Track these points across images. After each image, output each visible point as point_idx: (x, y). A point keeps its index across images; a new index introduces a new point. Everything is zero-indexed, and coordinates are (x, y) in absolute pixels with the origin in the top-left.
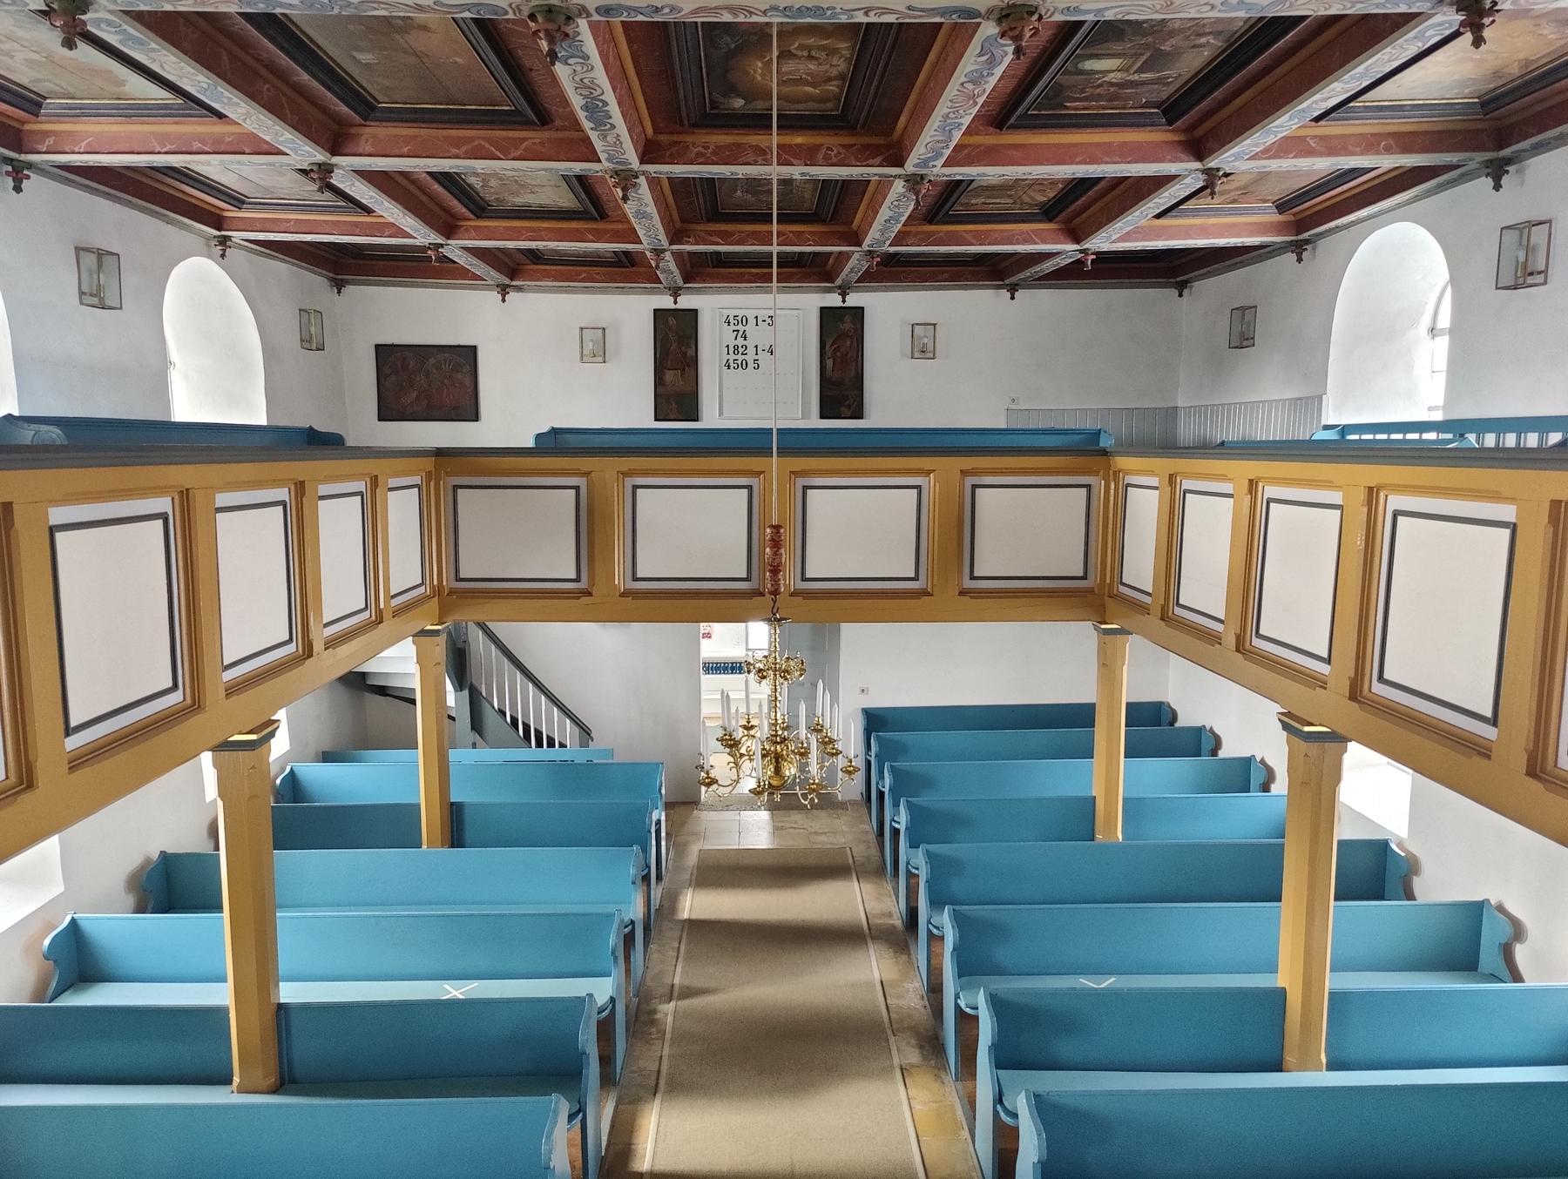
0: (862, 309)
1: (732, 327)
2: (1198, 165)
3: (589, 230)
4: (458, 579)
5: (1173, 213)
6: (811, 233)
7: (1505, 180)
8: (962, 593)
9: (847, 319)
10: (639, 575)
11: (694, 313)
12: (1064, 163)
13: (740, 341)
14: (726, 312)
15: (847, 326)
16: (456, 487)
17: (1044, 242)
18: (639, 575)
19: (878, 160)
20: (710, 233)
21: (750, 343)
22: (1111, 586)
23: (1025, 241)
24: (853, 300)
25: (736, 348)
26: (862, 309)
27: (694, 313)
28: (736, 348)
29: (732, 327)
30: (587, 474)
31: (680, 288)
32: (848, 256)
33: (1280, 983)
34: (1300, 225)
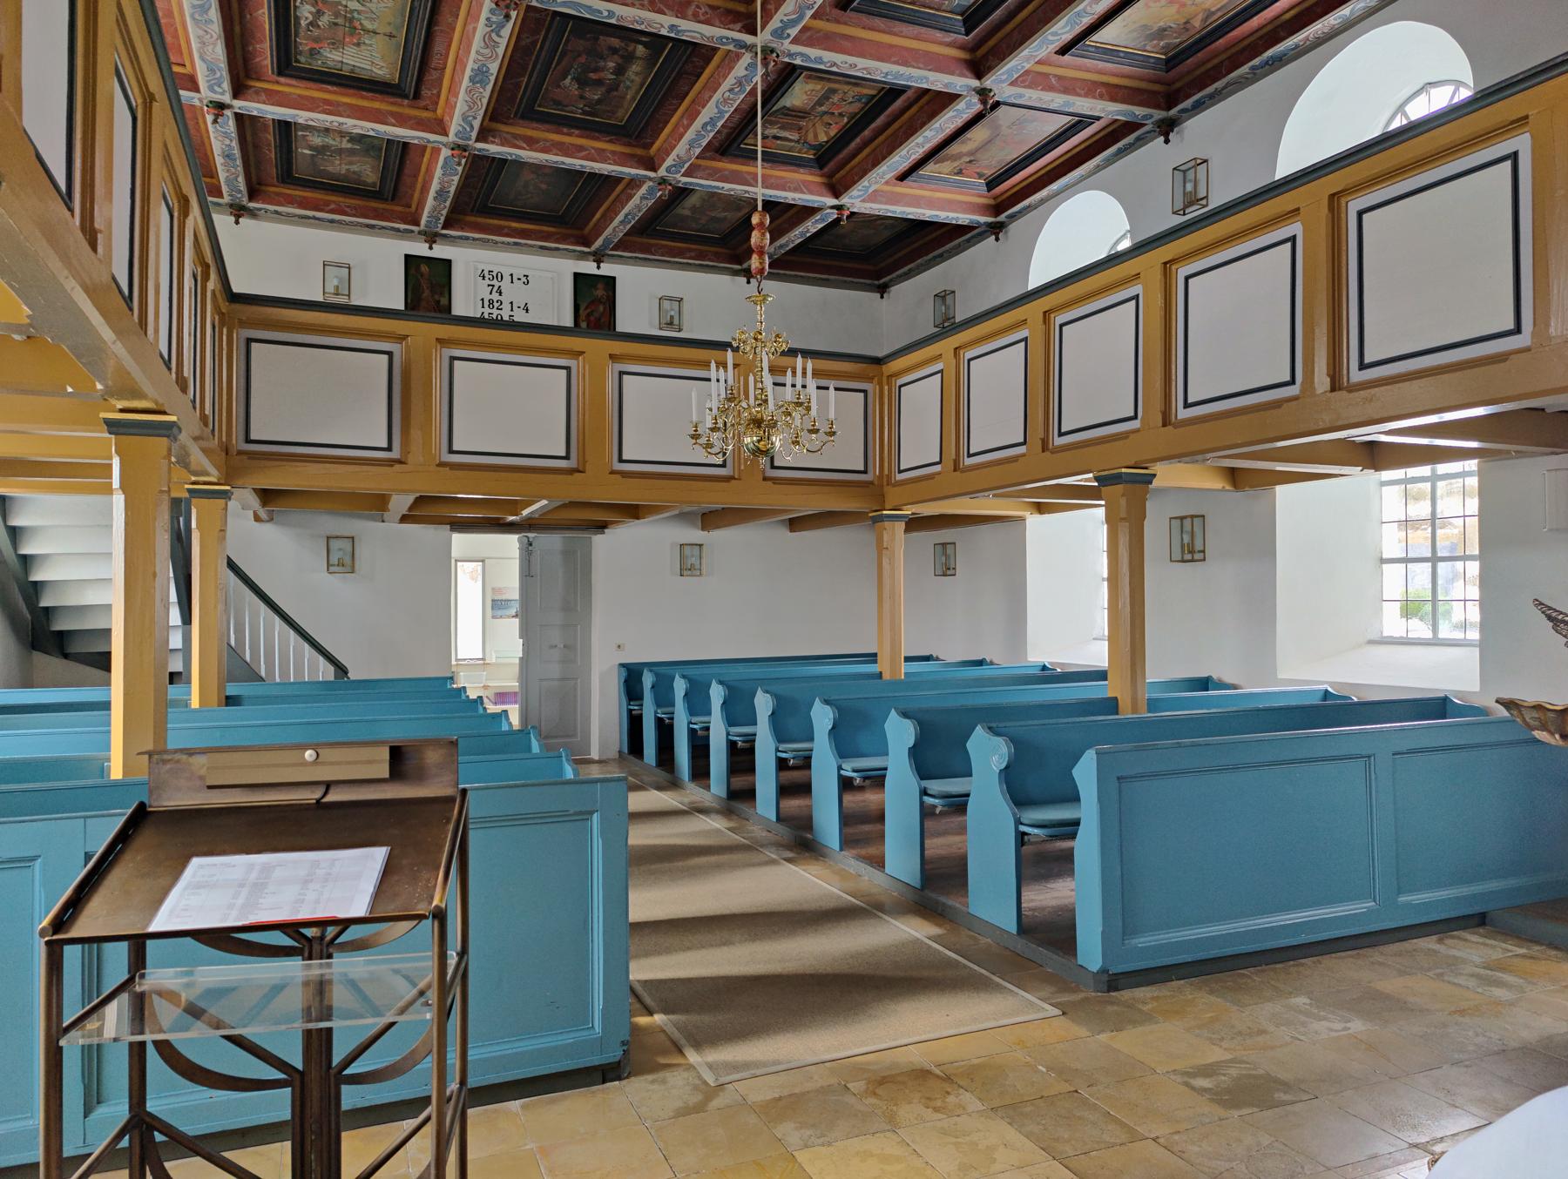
0: (614, 278)
1: (487, 282)
2: (975, 83)
3: (392, 114)
4: (248, 441)
5: (913, 177)
6: (613, 153)
7: (1171, 136)
8: (765, 479)
9: (600, 286)
10: (455, 448)
11: (448, 263)
12: (882, 60)
13: (495, 296)
14: (481, 267)
15: (600, 292)
16: (249, 341)
17: (811, 193)
18: (455, 448)
19: (738, 26)
20: (516, 136)
21: (505, 299)
22: (889, 476)
23: (795, 190)
24: (607, 269)
25: (491, 302)
26: (614, 278)
27: (448, 263)
28: (491, 302)
29: (487, 282)
30: (402, 338)
31: (436, 235)
32: (635, 183)
33: (1110, 694)
34: (997, 209)
